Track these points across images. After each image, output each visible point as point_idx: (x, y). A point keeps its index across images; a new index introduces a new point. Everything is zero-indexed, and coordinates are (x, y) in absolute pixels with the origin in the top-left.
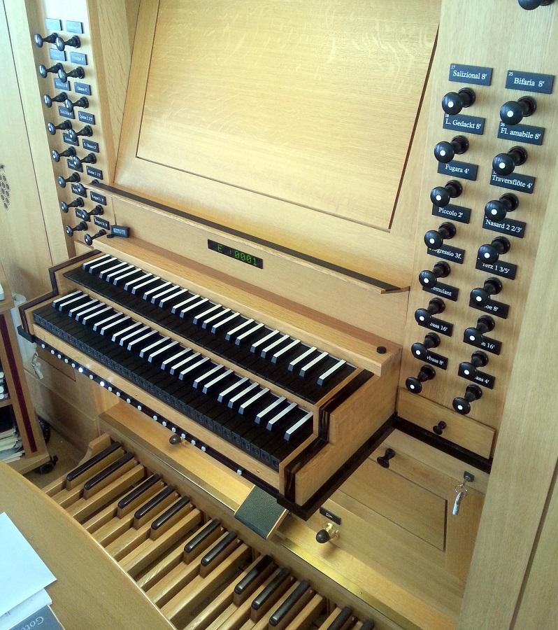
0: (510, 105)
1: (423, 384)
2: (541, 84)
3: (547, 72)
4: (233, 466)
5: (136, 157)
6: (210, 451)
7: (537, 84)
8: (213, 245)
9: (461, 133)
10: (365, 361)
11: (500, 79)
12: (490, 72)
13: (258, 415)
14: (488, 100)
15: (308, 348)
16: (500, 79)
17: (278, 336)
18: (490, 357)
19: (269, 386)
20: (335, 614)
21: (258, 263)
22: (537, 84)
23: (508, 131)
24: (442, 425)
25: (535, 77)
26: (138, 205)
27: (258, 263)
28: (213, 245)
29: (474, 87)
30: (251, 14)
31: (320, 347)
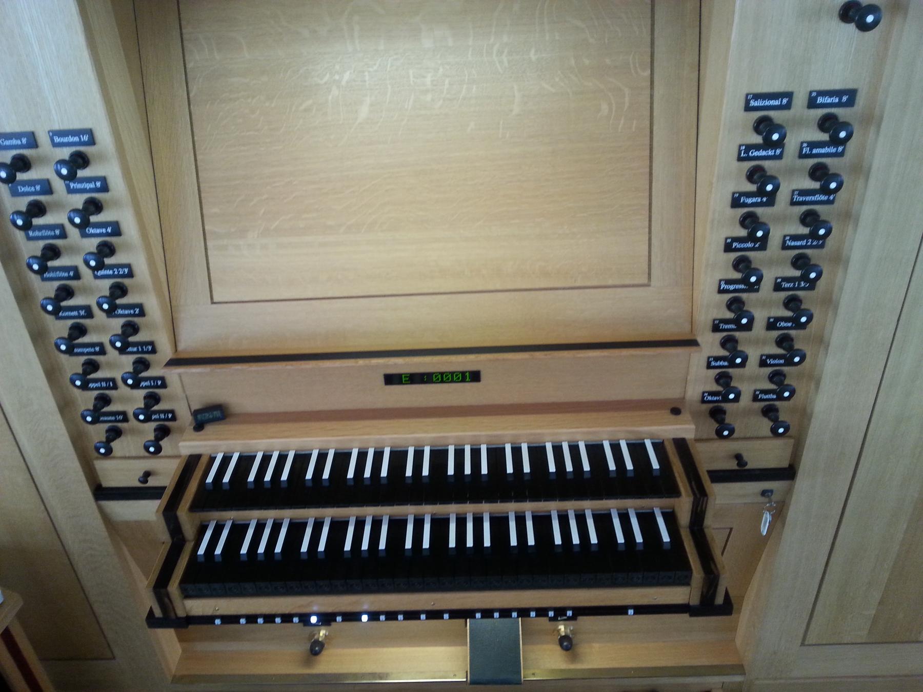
0: (62, 162)
1: (113, 444)
2: (845, 99)
3: (850, 86)
4: (620, 610)
5: (213, 303)
6: (641, 610)
7: (840, 99)
8: (391, 379)
9: (32, 198)
10: (677, 429)
11: (800, 101)
12: (789, 95)
13: (363, 549)
14: (43, 160)
15: (253, 458)
16: (800, 101)
17: (266, 459)
18: (785, 372)
19: (287, 515)
20: (738, 679)
21: (475, 376)
22: (840, 99)
23: (811, 150)
24: (147, 475)
25: (838, 93)
26: (289, 367)
27: (475, 376)
28: (391, 379)
29: (82, 149)
30: (371, 69)
31: (362, 446)
